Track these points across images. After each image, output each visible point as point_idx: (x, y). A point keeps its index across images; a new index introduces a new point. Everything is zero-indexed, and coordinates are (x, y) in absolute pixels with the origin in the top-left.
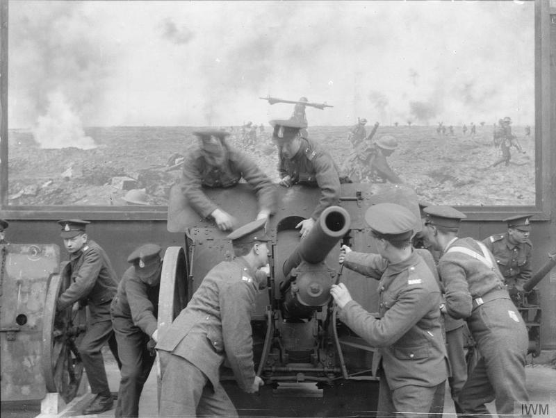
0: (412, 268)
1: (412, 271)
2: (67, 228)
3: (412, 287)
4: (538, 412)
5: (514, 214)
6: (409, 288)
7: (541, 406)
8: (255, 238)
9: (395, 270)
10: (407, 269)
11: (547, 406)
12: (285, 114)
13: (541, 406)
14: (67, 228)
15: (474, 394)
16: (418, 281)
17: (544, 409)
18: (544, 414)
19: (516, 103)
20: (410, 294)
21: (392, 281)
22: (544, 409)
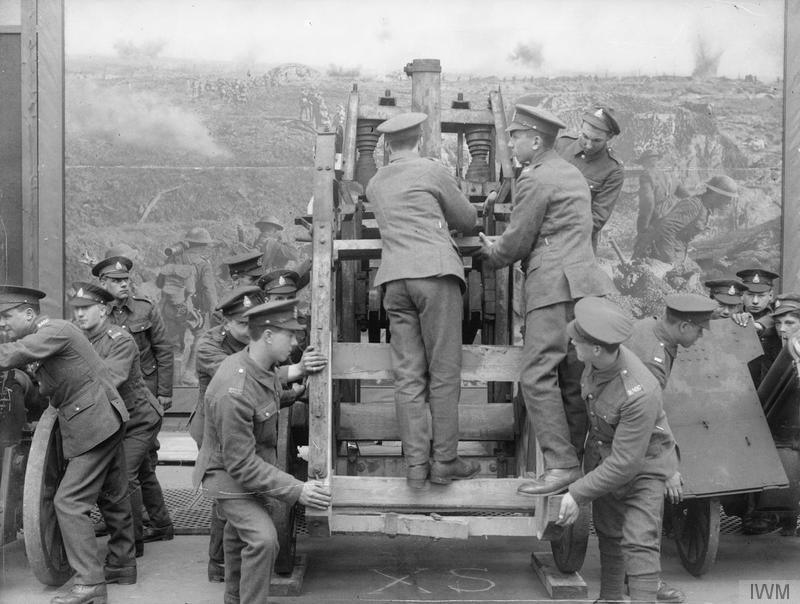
0: (625, 372)
1: (626, 375)
2: (756, 279)
3: (635, 398)
4: (774, 595)
5: (423, 235)
6: (631, 400)
7: (778, 586)
8: (268, 322)
9: (605, 378)
10: (619, 374)
11: (787, 586)
12: (461, 91)
13: (778, 586)
14: (756, 279)
15: (695, 93)
16: (637, 389)
17: (782, 591)
18: (782, 597)
19: (768, 69)
20: (633, 408)
21: (601, 391)
22: (782, 591)
